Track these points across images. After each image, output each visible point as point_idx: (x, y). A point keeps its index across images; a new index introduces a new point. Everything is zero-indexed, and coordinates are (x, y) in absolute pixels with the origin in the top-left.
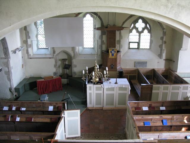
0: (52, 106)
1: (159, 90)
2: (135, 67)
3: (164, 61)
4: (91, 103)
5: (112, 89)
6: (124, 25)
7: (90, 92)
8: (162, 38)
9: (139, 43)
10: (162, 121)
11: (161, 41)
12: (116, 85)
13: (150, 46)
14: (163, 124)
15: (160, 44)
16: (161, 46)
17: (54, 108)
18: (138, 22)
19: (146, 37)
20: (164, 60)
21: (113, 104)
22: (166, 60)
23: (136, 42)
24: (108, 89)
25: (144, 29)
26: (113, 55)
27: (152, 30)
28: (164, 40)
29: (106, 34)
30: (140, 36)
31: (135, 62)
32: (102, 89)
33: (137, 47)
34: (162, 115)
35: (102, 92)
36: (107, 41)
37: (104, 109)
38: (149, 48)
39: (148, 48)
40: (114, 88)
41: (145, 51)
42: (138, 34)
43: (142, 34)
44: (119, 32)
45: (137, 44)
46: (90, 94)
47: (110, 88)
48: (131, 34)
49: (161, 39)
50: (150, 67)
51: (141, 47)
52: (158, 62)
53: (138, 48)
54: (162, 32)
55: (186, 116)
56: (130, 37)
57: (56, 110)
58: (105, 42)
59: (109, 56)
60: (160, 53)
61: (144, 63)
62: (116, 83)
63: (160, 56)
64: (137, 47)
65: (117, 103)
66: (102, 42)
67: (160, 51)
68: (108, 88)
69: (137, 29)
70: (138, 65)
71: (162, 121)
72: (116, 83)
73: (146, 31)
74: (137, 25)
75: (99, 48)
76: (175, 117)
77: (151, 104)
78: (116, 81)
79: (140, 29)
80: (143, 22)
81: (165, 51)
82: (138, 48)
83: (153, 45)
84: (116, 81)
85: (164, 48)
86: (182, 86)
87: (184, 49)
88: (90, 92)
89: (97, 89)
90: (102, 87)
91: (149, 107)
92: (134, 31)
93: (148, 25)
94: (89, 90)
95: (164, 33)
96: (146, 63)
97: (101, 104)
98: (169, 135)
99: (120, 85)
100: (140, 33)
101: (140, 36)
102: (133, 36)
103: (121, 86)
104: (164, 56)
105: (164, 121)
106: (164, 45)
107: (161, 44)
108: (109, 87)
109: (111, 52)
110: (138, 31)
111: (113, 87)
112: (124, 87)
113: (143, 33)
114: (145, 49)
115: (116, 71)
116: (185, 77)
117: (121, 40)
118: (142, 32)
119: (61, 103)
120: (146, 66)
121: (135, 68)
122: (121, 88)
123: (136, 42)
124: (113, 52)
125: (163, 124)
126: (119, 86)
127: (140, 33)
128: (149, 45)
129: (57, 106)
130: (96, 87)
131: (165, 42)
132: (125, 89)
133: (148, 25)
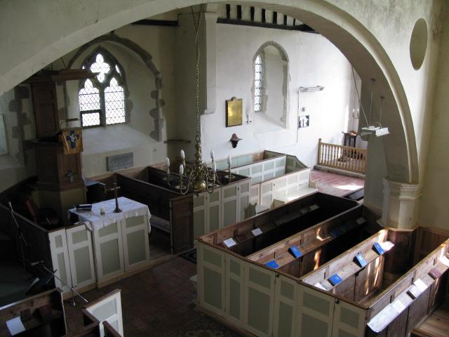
0: (15, 316)
1: (203, 204)
2: (108, 170)
3: (165, 146)
4: (64, 284)
5: (113, 228)
6: (73, 65)
7: (60, 250)
8: (155, 95)
9: (102, 112)
10: (290, 251)
11: (154, 100)
12: (121, 214)
13: (128, 116)
14: (295, 257)
15: (151, 108)
16: (154, 113)
17: (23, 321)
18: (94, 61)
19: (115, 94)
20: (165, 142)
21: (118, 267)
22: (169, 142)
23: (95, 111)
24: (104, 232)
25: (109, 77)
26: (73, 145)
27: (127, 77)
28: (160, 97)
29: (30, 96)
30: (102, 95)
31: (107, 158)
32: (89, 233)
33: (98, 123)
34: (288, 239)
35: (88, 243)
36: (35, 113)
37: (100, 287)
38: (123, 120)
39: (121, 122)
40: (116, 223)
41: (120, 129)
42: (96, 90)
43: (107, 90)
44: (62, 87)
45: (98, 114)
46: (61, 256)
47: (107, 226)
48: (82, 91)
49: (152, 96)
50: (139, 164)
51: (108, 122)
52: (155, 150)
53: (103, 123)
54: (154, 81)
55: (318, 227)
56: (82, 99)
57: (34, 323)
58: (28, 117)
59: (65, 150)
60: (153, 129)
61: (126, 158)
62: (117, 210)
63: (155, 135)
64: (98, 123)
65: (74, 276)
66: (22, 118)
67: (153, 124)
68: (104, 227)
69: (93, 77)
70: (116, 164)
71: (290, 251)
72: (117, 210)
73: (114, 81)
74: (94, 68)
75: (14, 137)
76: (305, 235)
77: (237, 230)
78: (117, 204)
79: (101, 79)
80: (106, 61)
81: (165, 123)
82: (103, 123)
83: (133, 112)
84: (117, 204)
85: (161, 116)
86: (239, 184)
87: (210, 111)
88: (60, 250)
89: (77, 238)
90: (87, 229)
91: (234, 238)
92: (88, 83)
93: (116, 67)
94: (57, 247)
95: (159, 82)
96: (131, 154)
97: (90, 277)
98: (338, 265)
99: (129, 212)
100: (101, 87)
101: (102, 95)
102: (87, 97)
103: (131, 216)
104: (164, 134)
105: (294, 250)
106: (161, 109)
107: (155, 107)
108: (106, 224)
109: (68, 138)
110: (96, 84)
111: (114, 222)
112: (137, 215)
113: (108, 88)
114: (116, 124)
115: (83, 185)
116: (239, 164)
117: (69, 108)
118: (107, 84)
119: (44, 296)
120: (132, 164)
121: (110, 173)
122: (132, 221)
123: (95, 111)
124: (73, 138)
125: (295, 257)
126: (127, 217)
127: (101, 87)
128: (122, 113)
129: (32, 310)
130: (74, 235)
131: (163, 103)
132: (139, 220)
133: (116, 67)
